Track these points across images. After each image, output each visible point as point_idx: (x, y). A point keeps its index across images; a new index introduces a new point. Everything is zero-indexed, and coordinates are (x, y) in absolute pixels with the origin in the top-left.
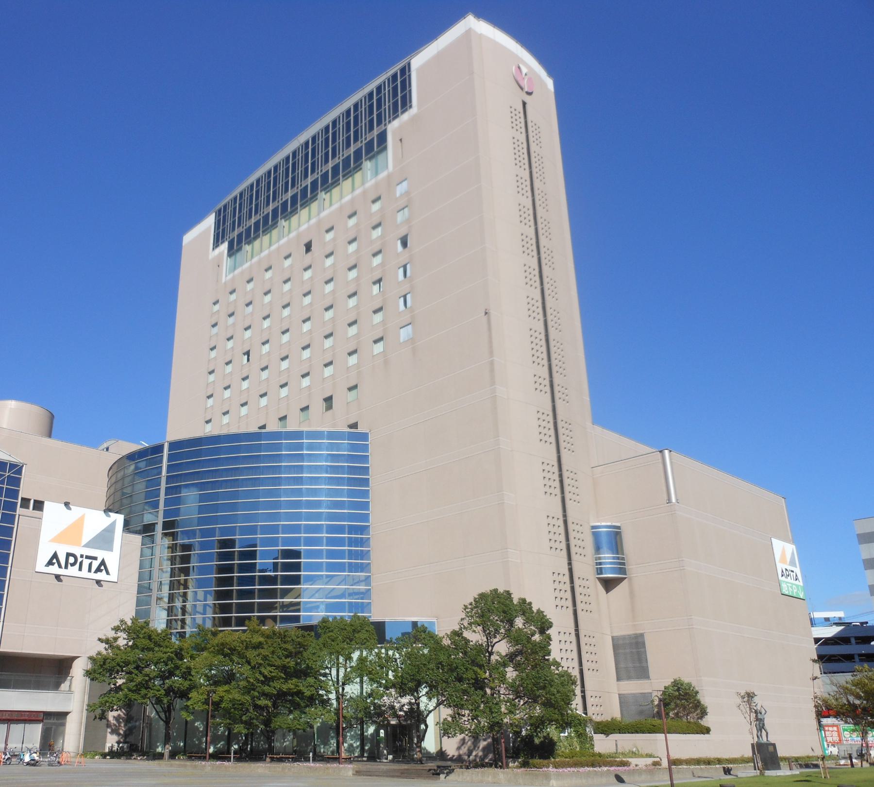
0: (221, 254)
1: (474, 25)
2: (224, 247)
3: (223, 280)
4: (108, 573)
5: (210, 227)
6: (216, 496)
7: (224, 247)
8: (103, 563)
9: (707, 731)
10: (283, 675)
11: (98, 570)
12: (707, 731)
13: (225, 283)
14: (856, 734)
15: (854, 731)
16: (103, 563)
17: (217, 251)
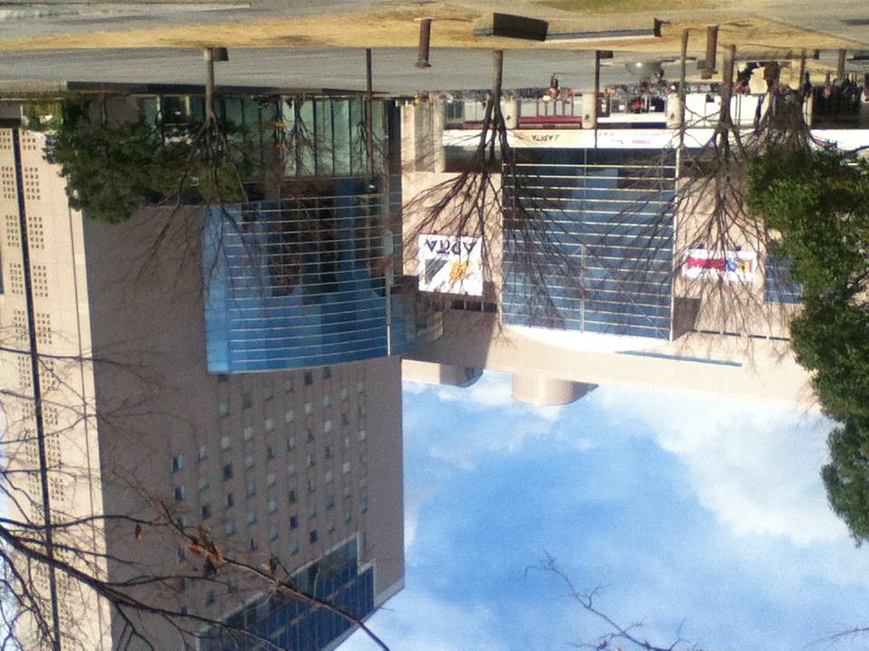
0: (364, 561)
1: (510, 146)
2: (362, 569)
3: (358, 534)
4: (427, 242)
5: (378, 592)
6: (342, 318)
7: (362, 569)
8: (432, 249)
9: (430, 66)
10: (382, 148)
11: (435, 243)
12: (430, 66)
13: (357, 530)
14: (749, 185)
15: (750, 183)
16: (432, 249)
17: (368, 566)
